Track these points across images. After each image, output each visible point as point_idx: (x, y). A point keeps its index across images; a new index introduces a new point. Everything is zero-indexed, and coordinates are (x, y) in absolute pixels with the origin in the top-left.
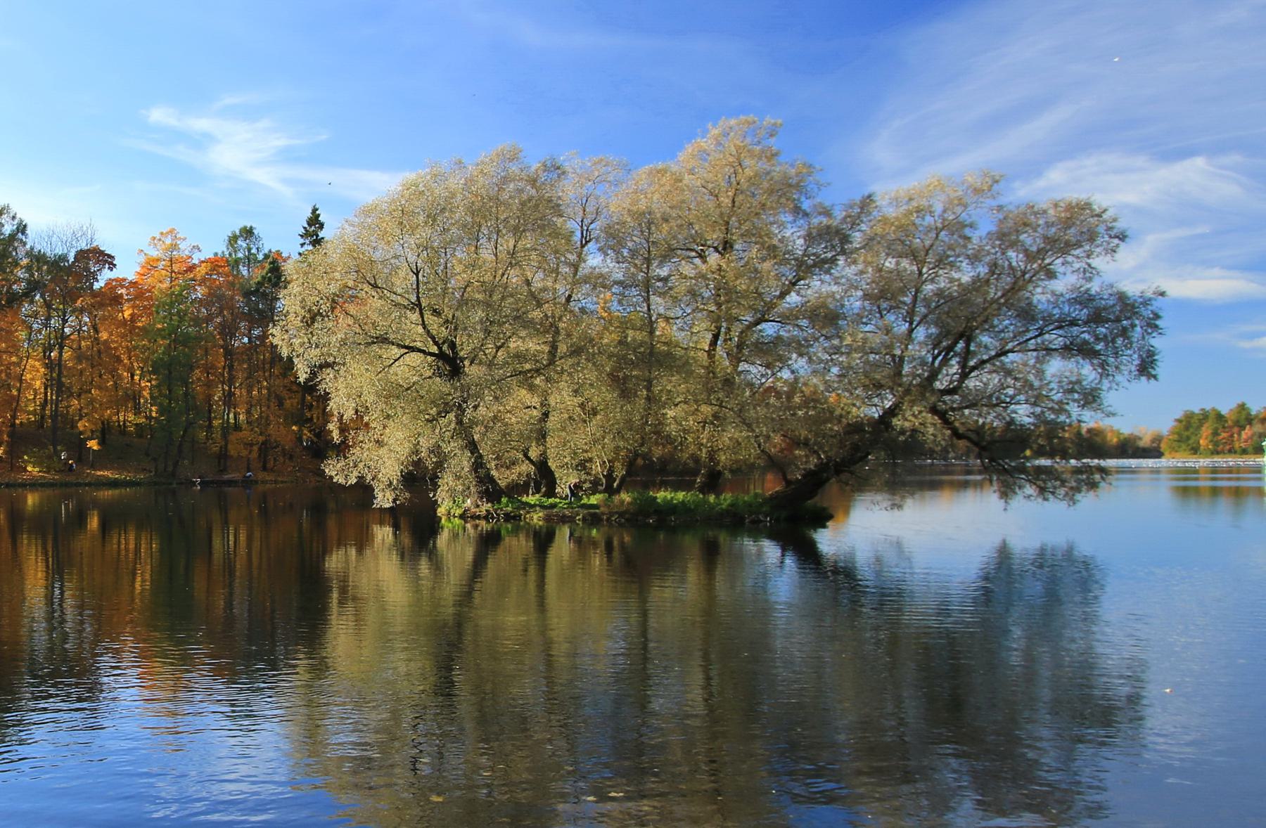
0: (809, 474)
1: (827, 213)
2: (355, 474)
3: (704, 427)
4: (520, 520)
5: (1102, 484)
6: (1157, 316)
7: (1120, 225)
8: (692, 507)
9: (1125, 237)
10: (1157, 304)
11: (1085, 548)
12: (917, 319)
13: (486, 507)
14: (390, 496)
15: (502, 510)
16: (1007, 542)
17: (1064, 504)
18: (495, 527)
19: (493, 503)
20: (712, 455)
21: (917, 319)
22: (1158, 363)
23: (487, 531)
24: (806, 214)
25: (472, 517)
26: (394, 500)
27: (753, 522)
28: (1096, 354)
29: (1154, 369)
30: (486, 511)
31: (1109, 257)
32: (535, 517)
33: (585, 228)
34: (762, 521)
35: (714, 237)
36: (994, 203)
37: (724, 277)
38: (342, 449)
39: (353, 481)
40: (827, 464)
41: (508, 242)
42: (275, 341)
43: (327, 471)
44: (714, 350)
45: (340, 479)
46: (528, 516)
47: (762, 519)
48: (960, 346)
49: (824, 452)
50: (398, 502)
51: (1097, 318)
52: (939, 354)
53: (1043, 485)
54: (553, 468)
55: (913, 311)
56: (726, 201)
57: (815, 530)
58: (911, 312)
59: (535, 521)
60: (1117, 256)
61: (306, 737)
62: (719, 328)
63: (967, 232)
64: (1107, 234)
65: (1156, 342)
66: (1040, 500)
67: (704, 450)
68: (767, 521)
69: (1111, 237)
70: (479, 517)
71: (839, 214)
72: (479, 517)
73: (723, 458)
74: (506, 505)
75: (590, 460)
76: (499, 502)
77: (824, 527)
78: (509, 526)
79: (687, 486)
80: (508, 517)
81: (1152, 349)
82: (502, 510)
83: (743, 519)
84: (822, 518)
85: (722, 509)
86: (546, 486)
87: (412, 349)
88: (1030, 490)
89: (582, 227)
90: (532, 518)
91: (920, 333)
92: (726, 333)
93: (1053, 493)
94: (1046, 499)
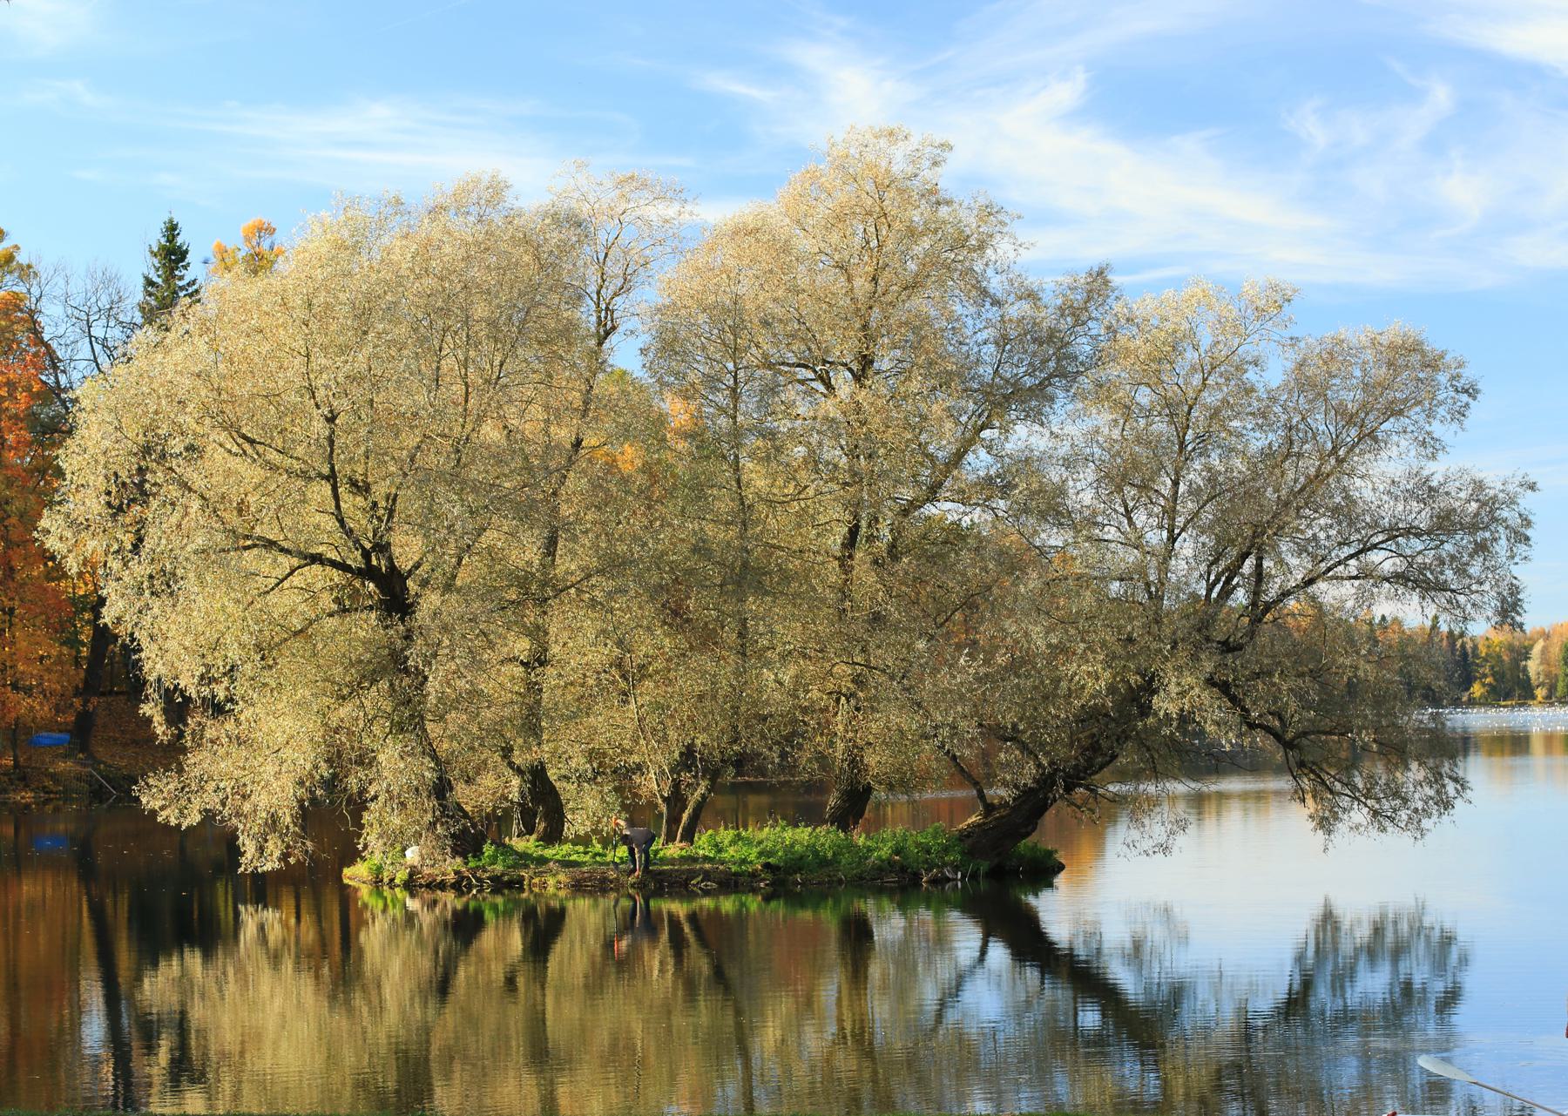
0: (1026, 794)
1: (1031, 296)
2: (197, 804)
3: (838, 701)
4: (522, 890)
5: (1458, 803)
6: (1528, 523)
7: (1468, 374)
8: (830, 855)
9: (1477, 391)
10: (1527, 501)
11: (1444, 912)
12: (1180, 521)
13: (451, 866)
14: (274, 847)
15: (485, 871)
16: (1332, 902)
17: (1406, 838)
18: (472, 905)
19: (465, 858)
20: (855, 762)
21: (1180, 521)
22: (1525, 606)
23: (455, 912)
24: (996, 303)
25: (428, 886)
26: (284, 857)
27: (934, 882)
28: (1442, 587)
29: (1519, 614)
30: (456, 873)
31: (1455, 425)
32: (551, 881)
33: (603, 306)
34: (948, 880)
35: (844, 349)
36: (1287, 333)
37: (863, 423)
38: (172, 755)
39: (194, 818)
40: (1052, 776)
41: (488, 356)
42: (52, 543)
43: (144, 800)
44: (851, 557)
45: (170, 816)
46: (536, 880)
47: (950, 876)
48: (1248, 566)
49: (1047, 754)
50: (292, 860)
51: (1445, 524)
52: (1217, 580)
53: (1377, 806)
54: (553, 778)
55: (1174, 510)
56: (861, 285)
57: (1036, 895)
58: (1170, 513)
59: (551, 890)
60: (1466, 422)
61: (673, 1077)
62: (856, 516)
63: (1251, 375)
64: (1452, 386)
65: (1522, 573)
66: (1374, 832)
67: (840, 746)
68: (956, 879)
69: (1457, 391)
70: (442, 886)
71: (1051, 300)
72: (442, 886)
73: (871, 759)
74: (492, 862)
75: (639, 767)
76: (478, 853)
77: (1050, 885)
78: (499, 900)
79: (811, 815)
80: (499, 885)
81: (1514, 582)
82: (485, 871)
83: (916, 877)
84: (1043, 872)
85: (879, 858)
86: (546, 817)
87: (316, 559)
88: (1360, 815)
89: (598, 305)
90: (544, 885)
91: (1186, 546)
92: (869, 526)
93: (1392, 819)
94: (1384, 830)
